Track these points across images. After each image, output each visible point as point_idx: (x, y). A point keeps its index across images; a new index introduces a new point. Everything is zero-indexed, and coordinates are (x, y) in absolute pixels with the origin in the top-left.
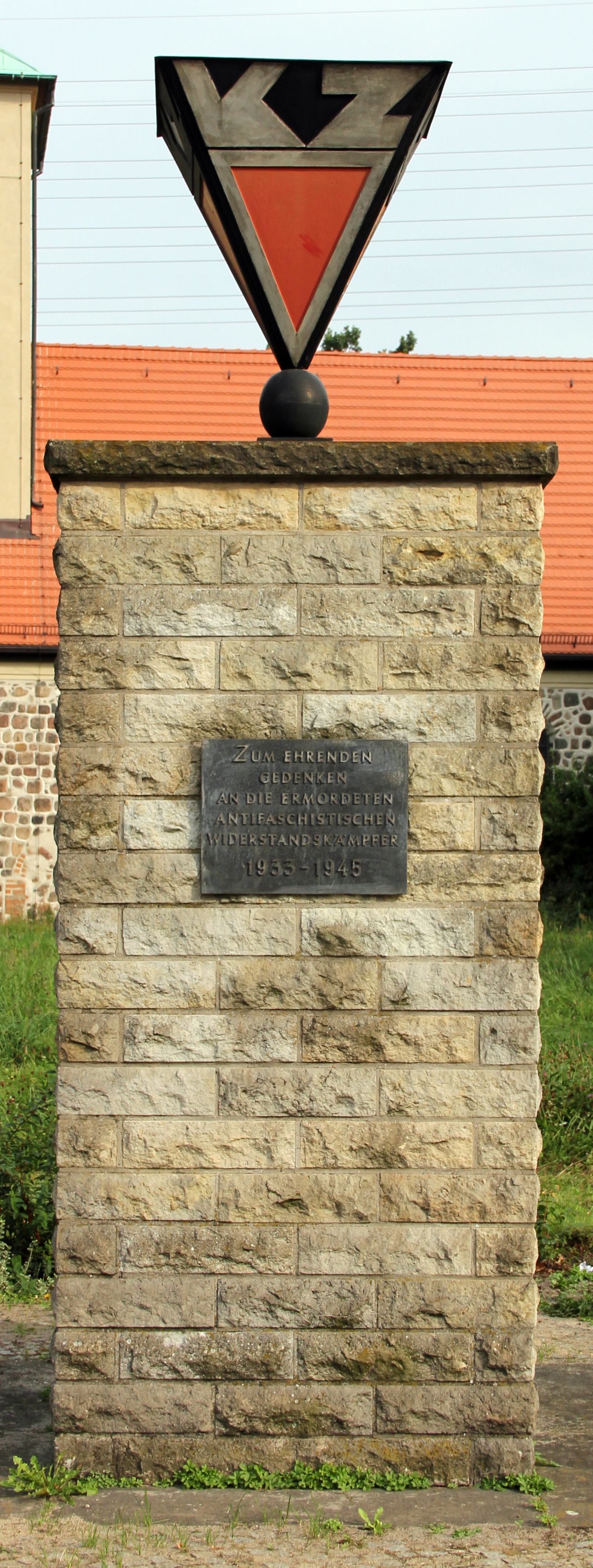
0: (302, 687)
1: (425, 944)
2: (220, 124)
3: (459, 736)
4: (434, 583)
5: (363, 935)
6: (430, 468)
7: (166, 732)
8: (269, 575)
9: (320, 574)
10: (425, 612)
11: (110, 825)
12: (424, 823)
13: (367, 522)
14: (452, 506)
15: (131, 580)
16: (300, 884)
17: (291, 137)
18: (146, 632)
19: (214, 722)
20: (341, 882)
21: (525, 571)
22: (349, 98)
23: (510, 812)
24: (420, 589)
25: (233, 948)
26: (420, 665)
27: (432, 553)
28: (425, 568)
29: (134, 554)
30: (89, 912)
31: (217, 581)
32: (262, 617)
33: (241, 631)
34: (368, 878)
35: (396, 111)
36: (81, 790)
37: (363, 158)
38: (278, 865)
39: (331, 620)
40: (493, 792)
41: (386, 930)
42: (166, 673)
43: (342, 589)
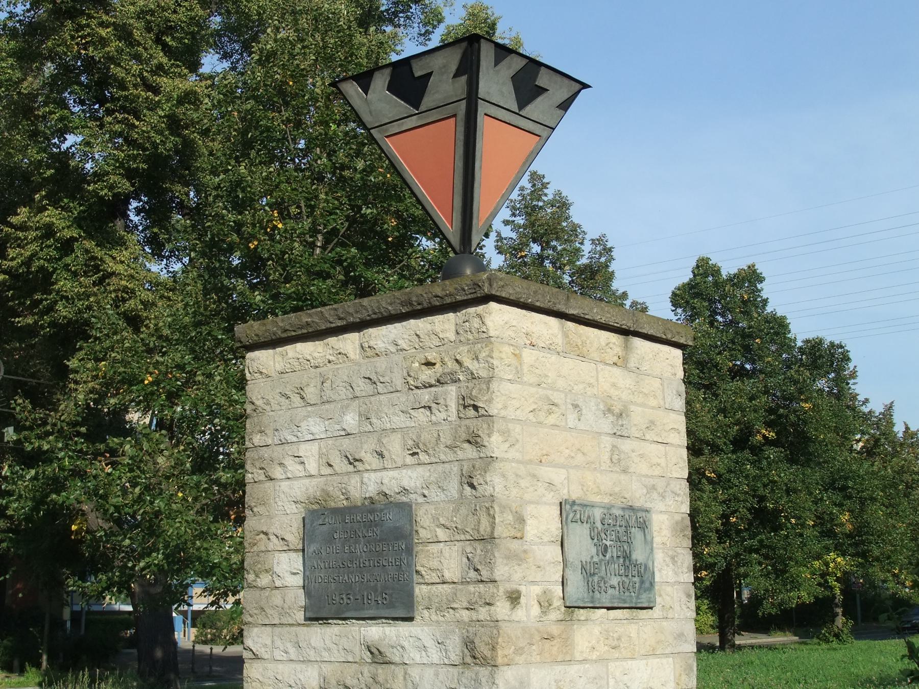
0: (361, 469)
1: (429, 654)
2: (371, 112)
3: (447, 496)
4: (431, 386)
5: (393, 647)
6: (419, 304)
7: (294, 507)
8: (344, 393)
9: (369, 388)
10: (424, 407)
11: (267, 571)
12: (425, 562)
13: (393, 349)
14: (438, 328)
15: (278, 407)
16: (356, 610)
17: (408, 109)
18: (284, 441)
19: (315, 498)
20: (378, 609)
21: (484, 368)
22: (429, 75)
23: (479, 551)
24: (425, 390)
25: (326, 656)
26: (421, 446)
27: (429, 364)
28: (427, 375)
29: (278, 391)
30: (256, 630)
31: (319, 402)
32: (338, 423)
33: (329, 434)
34: (391, 605)
35: (456, 76)
36: (255, 548)
37: (449, 110)
38: (344, 596)
39: (374, 420)
40: (469, 537)
41: (406, 644)
42: (293, 467)
43: (382, 397)
